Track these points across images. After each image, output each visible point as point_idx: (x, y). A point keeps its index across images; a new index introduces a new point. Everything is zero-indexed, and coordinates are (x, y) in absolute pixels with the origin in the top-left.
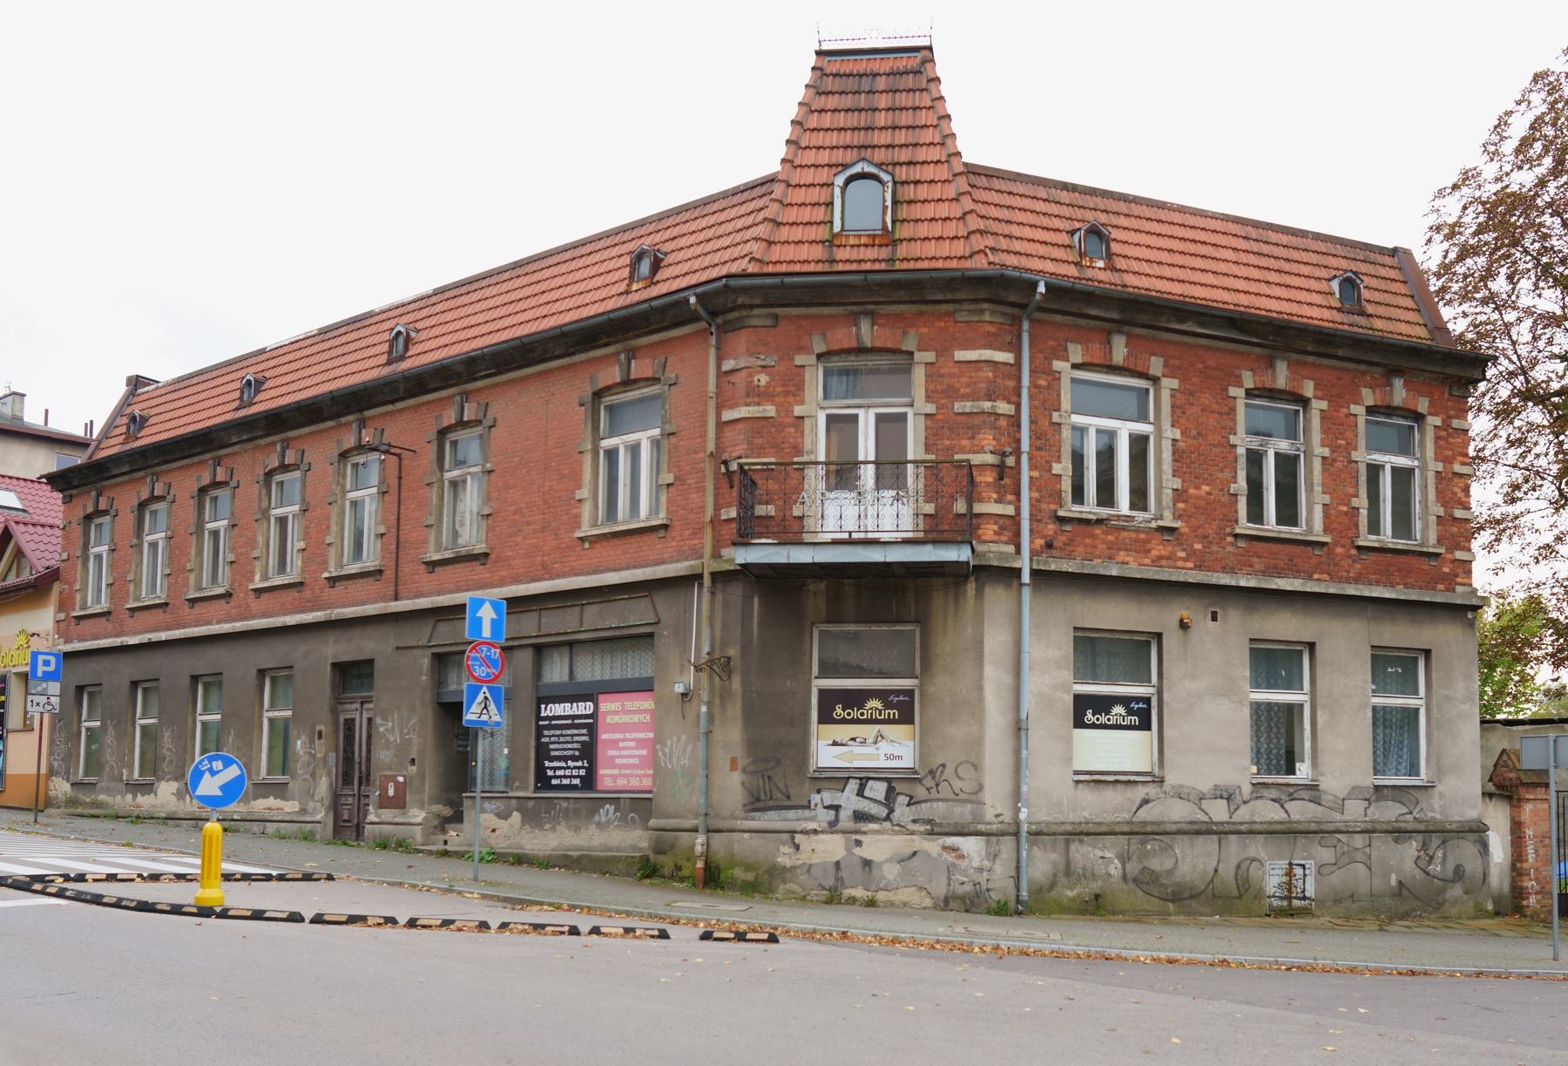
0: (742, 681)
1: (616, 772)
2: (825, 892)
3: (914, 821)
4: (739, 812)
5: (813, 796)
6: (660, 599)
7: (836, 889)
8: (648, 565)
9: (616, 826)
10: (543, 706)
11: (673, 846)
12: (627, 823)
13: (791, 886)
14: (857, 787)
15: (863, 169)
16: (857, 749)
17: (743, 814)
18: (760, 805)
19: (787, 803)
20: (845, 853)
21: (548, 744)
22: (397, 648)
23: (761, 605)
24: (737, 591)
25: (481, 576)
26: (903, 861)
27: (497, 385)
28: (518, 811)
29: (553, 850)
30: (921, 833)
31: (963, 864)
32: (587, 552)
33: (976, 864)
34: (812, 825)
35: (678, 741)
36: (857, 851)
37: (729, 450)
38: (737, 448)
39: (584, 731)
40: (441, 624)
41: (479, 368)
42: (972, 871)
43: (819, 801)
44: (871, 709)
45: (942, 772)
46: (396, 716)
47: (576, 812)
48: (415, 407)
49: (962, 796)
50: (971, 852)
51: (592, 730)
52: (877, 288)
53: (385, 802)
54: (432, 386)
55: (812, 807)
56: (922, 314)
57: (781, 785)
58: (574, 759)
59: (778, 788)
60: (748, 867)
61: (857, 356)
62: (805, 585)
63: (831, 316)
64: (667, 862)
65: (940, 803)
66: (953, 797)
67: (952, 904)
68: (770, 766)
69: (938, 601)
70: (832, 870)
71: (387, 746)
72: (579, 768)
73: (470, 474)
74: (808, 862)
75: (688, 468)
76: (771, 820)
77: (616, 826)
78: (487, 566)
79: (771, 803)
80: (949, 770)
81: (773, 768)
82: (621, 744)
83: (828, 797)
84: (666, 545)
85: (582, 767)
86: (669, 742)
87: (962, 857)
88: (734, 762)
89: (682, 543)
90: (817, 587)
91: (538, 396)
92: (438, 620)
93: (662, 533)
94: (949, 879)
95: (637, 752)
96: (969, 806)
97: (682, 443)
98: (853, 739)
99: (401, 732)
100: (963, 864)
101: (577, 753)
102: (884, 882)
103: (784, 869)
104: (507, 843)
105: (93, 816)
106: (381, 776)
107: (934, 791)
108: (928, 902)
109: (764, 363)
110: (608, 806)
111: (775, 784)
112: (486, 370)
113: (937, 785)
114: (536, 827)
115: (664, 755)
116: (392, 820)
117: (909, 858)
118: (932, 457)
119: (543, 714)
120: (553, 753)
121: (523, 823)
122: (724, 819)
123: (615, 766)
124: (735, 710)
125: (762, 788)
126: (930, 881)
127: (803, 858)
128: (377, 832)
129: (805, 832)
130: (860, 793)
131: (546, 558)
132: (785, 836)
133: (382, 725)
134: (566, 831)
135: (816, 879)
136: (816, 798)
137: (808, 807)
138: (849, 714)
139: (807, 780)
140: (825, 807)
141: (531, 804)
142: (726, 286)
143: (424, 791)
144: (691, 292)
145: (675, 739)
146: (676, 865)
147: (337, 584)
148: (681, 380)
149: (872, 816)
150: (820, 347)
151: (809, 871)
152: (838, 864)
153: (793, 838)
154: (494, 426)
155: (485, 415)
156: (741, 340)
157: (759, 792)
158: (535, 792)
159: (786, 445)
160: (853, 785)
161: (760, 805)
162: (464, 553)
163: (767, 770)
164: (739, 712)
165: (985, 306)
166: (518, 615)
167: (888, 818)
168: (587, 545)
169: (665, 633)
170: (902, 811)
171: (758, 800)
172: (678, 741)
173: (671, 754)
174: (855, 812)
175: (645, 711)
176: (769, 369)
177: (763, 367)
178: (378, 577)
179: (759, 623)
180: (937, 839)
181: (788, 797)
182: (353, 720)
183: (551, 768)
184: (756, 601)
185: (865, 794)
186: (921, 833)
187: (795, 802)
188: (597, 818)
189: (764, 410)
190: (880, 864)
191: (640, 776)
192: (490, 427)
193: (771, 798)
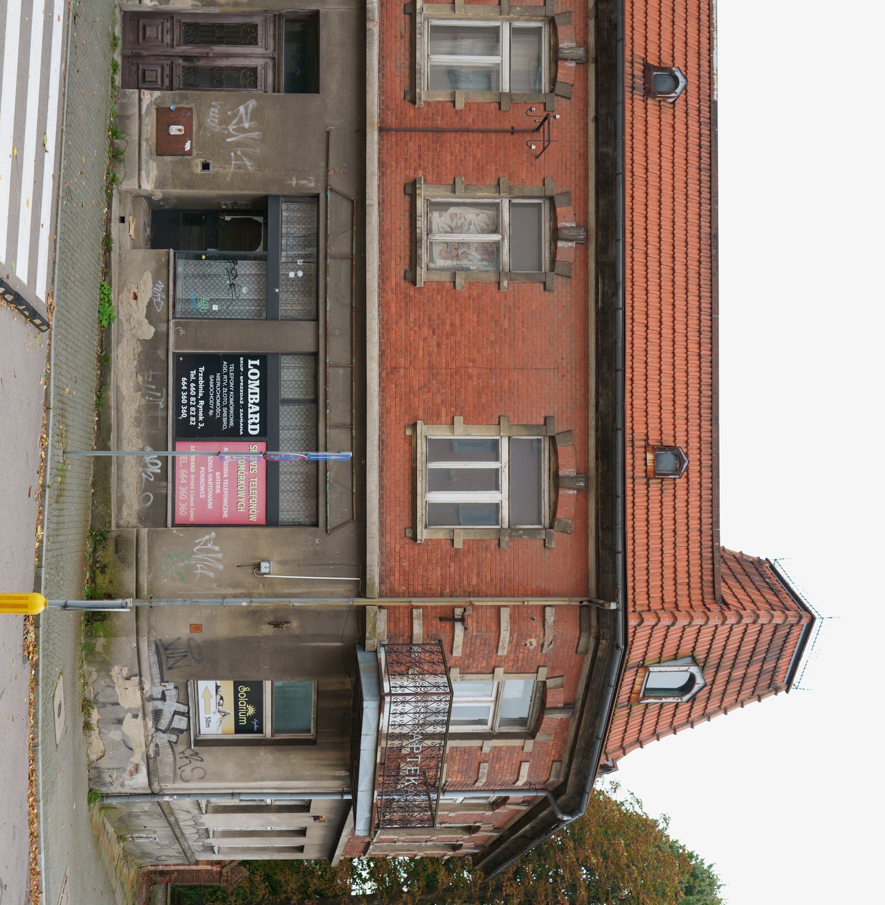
0: (269, 636)
1: (193, 470)
2: (92, 696)
3: (157, 745)
4: (155, 636)
5: (172, 684)
6: (347, 533)
7: (97, 702)
8: (381, 514)
9: (140, 476)
10: (257, 362)
11: (123, 560)
12: (144, 492)
13: (95, 675)
14: (182, 710)
15: (698, 684)
16: (213, 701)
17: (152, 639)
18: (162, 650)
19: (165, 668)
20: (126, 708)
21: (220, 371)
22: (328, 133)
23: (337, 647)
24: (348, 628)
25: (393, 272)
26: (124, 742)
27: (587, 291)
28: (156, 334)
29: (118, 387)
30: (147, 752)
31: (126, 775)
32: (402, 431)
33: (126, 782)
34: (147, 687)
35: (218, 560)
36: (129, 715)
37: (475, 614)
38: (475, 624)
39: (232, 424)
40: (350, 204)
41: (607, 282)
42: (121, 781)
43: (168, 688)
44: (247, 709)
45: (197, 760)
46: (255, 135)
47: (153, 421)
48: (585, 156)
49: (179, 772)
50: (135, 780)
51: (235, 434)
52: (590, 731)
53: (165, 117)
54: (602, 203)
55: (163, 684)
56: (565, 742)
57: (179, 664)
58: (206, 408)
59: (177, 662)
60: (107, 648)
61: (539, 698)
62: (349, 676)
63: (576, 687)
64: (107, 555)
65: (172, 759)
66: (178, 767)
67: (93, 772)
68: (196, 656)
69: (332, 755)
70: (112, 700)
71: (225, 121)
72: (197, 416)
73: (503, 239)
74: (116, 685)
75: (465, 564)
76: (149, 657)
77: (140, 476)
78: (403, 281)
79: (164, 657)
80: (199, 764)
81: (194, 658)
82: (218, 474)
83: (171, 693)
84: (398, 536)
85: (197, 421)
86: (217, 548)
87: (131, 775)
88: (196, 628)
89: (397, 559)
90: (348, 683)
91: (564, 356)
92: (353, 202)
93: (409, 533)
94: (113, 769)
95: (210, 495)
96: (171, 775)
97: (489, 555)
98: (222, 698)
99: (238, 144)
100: (126, 775)
101: (211, 412)
102: (106, 731)
103: (108, 672)
104: (124, 321)
105: (53, 278)
106: (191, 109)
107: (182, 755)
108: (93, 757)
109: (545, 647)
110: (160, 464)
111: (180, 660)
112: (603, 292)
113: (186, 757)
114: (140, 363)
115: (206, 544)
116: (144, 137)
117: (126, 746)
118: (447, 751)
119: (250, 362)
120: (211, 377)
121: (144, 342)
122: (149, 618)
123: (198, 465)
124: (243, 629)
125: (175, 651)
126: (110, 758)
127: (119, 682)
128: (130, 112)
129: (141, 683)
130: (176, 713)
131: (402, 371)
132: (136, 670)
133: (246, 109)
134: (136, 407)
135: (103, 691)
136: (171, 686)
137: (162, 681)
138: (242, 695)
139: (185, 680)
140: (163, 692)
141: (161, 353)
142: (618, 647)
143: (175, 187)
144: (621, 606)
145: (220, 556)
146: (105, 566)
147: (407, 17)
148: (547, 551)
149: (159, 720)
150: (550, 683)
151: (109, 686)
152: (118, 704)
153: (135, 676)
154: (545, 289)
155: (558, 274)
156: (570, 631)
157: (172, 649)
158: (174, 353)
159: (471, 661)
160: (183, 708)
161: (162, 650)
162: (419, 251)
163: (192, 653)
164: (241, 634)
165: (561, 780)
166: (349, 333)
167: (157, 730)
168: (409, 432)
169: (317, 541)
170: (163, 739)
171: (166, 649)
172: (218, 560)
173: (208, 551)
174: (161, 710)
175: (248, 506)
176: (539, 649)
177: (543, 645)
178: (408, 97)
179: (318, 646)
180: (142, 760)
181: (170, 668)
182: (253, 41)
183: (197, 376)
184: (339, 644)
185: (176, 716)
186: (147, 752)
187: (166, 673)
188: (148, 449)
189: (504, 649)
190: (120, 729)
191: (188, 501)
192: (545, 283)
193: (168, 657)
